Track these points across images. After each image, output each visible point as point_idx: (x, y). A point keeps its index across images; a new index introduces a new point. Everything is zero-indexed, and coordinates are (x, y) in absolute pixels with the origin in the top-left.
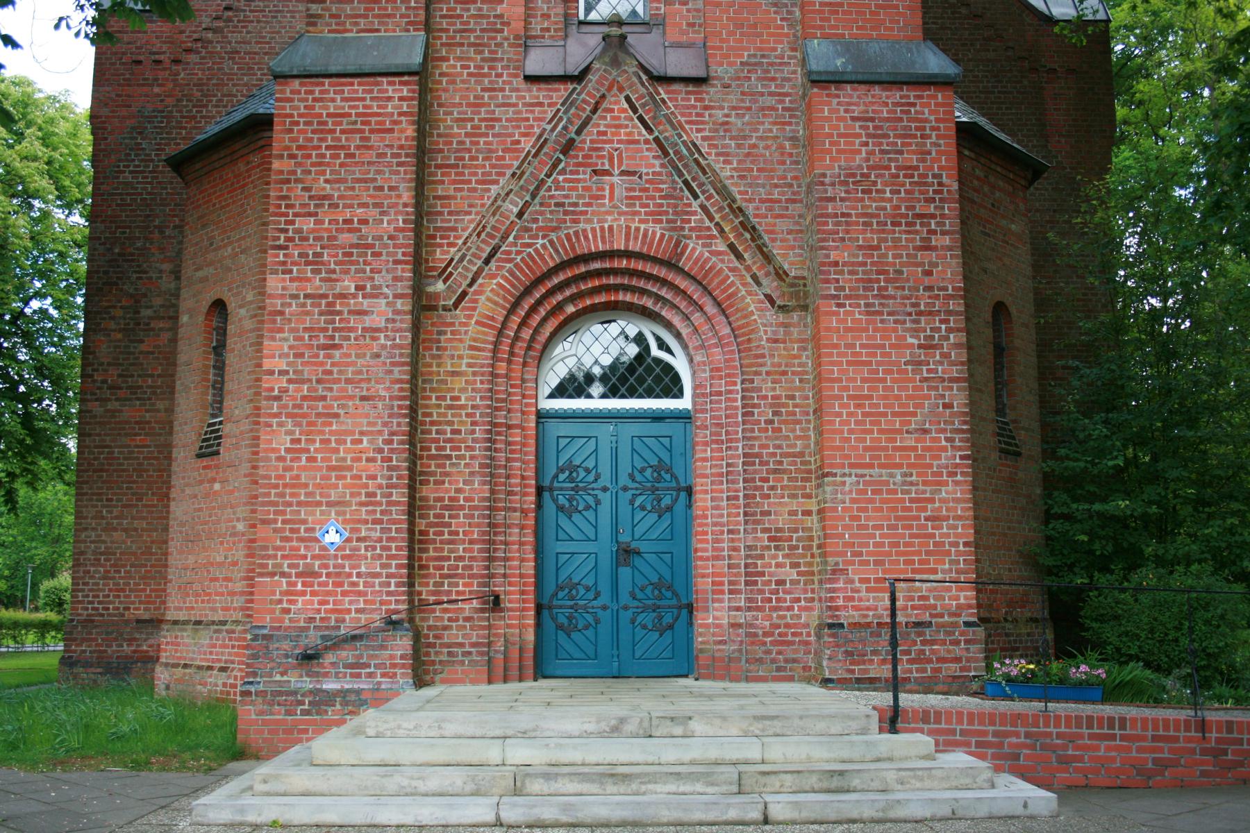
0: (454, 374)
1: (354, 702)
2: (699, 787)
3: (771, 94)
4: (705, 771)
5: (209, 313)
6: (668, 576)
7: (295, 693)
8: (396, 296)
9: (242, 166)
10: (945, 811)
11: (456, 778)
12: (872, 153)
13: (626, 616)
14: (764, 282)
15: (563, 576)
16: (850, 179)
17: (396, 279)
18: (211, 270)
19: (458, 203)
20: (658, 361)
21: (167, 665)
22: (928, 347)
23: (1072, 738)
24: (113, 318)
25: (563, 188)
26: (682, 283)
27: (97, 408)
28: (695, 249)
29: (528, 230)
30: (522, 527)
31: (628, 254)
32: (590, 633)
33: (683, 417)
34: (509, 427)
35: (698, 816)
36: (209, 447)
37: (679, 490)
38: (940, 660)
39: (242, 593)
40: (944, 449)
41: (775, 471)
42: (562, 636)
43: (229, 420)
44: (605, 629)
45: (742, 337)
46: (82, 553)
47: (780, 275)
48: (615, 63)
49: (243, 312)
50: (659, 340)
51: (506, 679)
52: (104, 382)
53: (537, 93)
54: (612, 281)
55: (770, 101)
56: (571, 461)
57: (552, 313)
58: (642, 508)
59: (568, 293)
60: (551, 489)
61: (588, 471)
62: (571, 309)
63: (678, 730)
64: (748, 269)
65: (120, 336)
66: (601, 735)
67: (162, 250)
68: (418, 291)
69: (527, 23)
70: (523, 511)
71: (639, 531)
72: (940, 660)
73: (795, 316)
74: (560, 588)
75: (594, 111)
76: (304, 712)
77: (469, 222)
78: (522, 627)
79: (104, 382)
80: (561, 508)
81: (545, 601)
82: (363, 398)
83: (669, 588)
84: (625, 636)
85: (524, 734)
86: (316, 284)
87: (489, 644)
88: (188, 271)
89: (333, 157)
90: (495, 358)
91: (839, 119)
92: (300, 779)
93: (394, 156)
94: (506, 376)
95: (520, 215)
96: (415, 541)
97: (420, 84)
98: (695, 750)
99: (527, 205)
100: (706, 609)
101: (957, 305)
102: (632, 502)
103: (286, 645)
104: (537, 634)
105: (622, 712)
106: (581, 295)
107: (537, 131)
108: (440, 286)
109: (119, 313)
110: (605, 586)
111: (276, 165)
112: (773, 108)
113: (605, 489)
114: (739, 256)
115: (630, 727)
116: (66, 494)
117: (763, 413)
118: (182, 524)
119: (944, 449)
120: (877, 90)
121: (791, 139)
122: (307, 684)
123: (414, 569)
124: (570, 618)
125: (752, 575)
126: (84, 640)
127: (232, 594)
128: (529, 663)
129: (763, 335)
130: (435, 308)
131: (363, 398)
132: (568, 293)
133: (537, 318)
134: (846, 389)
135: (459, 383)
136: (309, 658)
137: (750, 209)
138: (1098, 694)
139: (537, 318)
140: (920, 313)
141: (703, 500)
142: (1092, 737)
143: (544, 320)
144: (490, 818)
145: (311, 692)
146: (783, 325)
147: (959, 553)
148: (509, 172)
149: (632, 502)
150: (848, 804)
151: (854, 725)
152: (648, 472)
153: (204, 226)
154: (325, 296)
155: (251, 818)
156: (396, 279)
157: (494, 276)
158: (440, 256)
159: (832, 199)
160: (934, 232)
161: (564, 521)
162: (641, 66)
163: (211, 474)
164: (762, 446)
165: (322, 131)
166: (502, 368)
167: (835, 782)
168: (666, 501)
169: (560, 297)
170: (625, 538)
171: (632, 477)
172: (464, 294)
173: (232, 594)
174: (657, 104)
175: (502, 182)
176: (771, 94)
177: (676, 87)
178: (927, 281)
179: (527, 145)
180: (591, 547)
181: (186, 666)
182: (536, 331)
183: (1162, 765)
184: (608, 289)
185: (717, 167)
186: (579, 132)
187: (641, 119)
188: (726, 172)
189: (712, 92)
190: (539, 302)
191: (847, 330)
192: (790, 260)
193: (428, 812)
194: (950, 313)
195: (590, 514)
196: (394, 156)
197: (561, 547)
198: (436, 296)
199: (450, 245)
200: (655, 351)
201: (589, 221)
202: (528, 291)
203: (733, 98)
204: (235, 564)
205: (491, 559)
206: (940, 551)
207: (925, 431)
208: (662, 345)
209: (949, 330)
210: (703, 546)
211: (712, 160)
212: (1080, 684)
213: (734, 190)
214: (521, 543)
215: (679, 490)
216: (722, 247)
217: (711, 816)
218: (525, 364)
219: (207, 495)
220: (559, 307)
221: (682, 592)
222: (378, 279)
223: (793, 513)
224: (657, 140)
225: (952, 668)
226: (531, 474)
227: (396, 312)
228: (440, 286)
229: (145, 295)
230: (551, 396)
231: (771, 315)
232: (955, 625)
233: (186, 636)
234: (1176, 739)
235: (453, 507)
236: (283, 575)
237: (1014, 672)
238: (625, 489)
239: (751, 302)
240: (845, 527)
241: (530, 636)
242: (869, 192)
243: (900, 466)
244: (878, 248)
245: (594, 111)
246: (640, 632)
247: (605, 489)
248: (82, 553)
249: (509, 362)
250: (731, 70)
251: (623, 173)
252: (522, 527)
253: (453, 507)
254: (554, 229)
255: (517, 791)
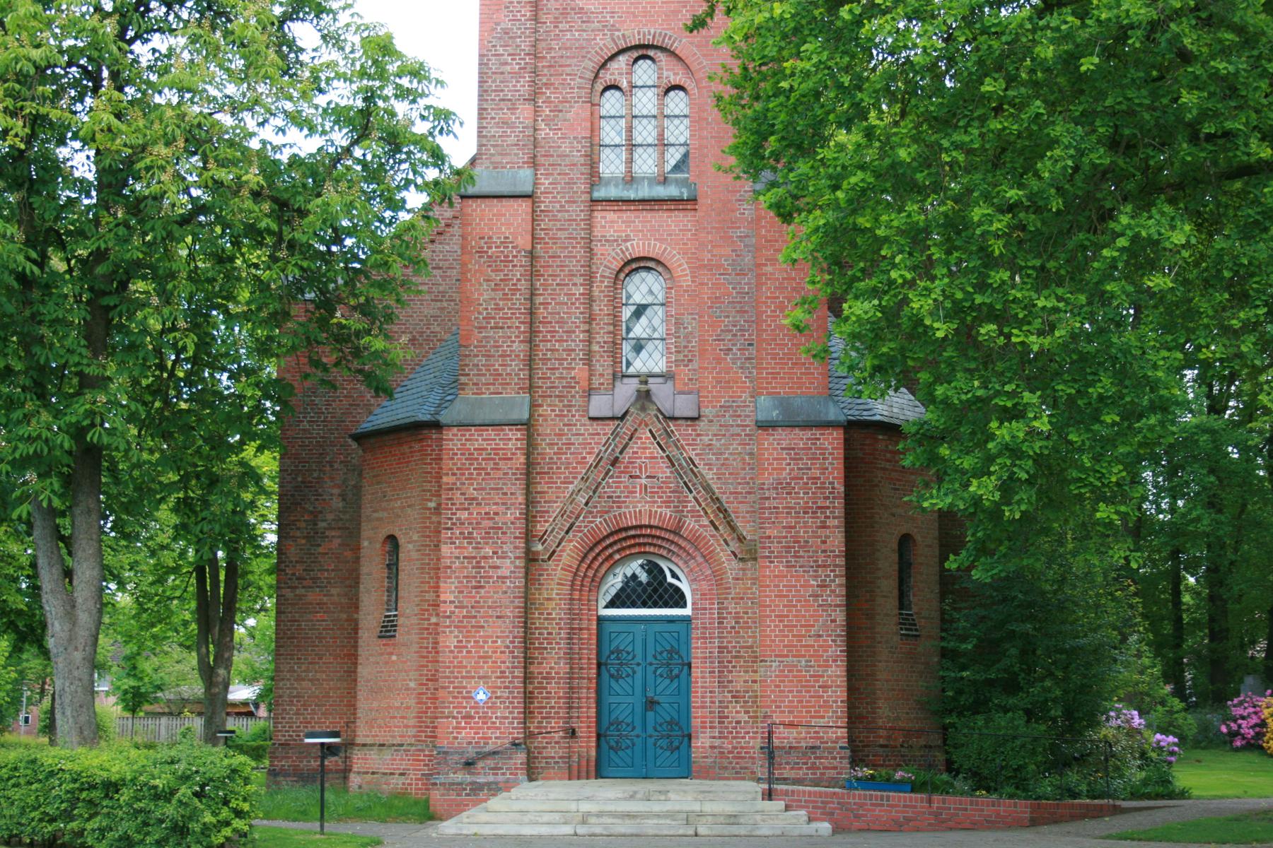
0: (549, 599)
1: (494, 789)
2: (668, 821)
3: (738, 426)
4: (670, 815)
5: (384, 542)
6: (676, 717)
7: (460, 784)
8: (517, 558)
9: (406, 449)
10: (779, 832)
11: (557, 817)
12: (792, 469)
13: (650, 741)
14: (731, 543)
15: (613, 717)
16: (779, 486)
17: (516, 548)
18: (385, 514)
19: (551, 495)
20: (671, 585)
21: (359, 773)
22: (823, 586)
23: (861, 805)
24: (298, 529)
25: (613, 486)
26: (683, 544)
27: (289, 594)
28: (690, 523)
29: (591, 512)
30: (589, 688)
31: (651, 527)
32: (629, 751)
33: (686, 620)
34: (581, 629)
35: (665, 832)
36: (388, 630)
37: (683, 665)
38: (825, 768)
39: (414, 727)
40: (830, 646)
41: (736, 657)
42: (612, 753)
43: (402, 616)
44: (638, 748)
45: (718, 576)
46: (280, 697)
47: (741, 539)
48: (643, 409)
49: (410, 546)
50: (671, 571)
51: (579, 778)
52: (294, 574)
53: (597, 427)
54: (641, 540)
55: (738, 430)
56: (618, 647)
57: (607, 559)
58: (661, 676)
59: (615, 548)
60: (606, 664)
61: (628, 653)
62: (617, 557)
63: (663, 798)
64: (721, 535)
65: (303, 541)
66: (625, 799)
67: (332, 479)
68: (528, 551)
69: (590, 380)
70: (589, 679)
71: (659, 689)
72: (825, 768)
73: (749, 564)
74: (611, 724)
75: (630, 439)
76: (467, 795)
77: (556, 508)
78: (588, 747)
79: (294, 574)
80: (612, 676)
81: (602, 732)
82: (498, 617)
83: (677, 724)
84: (650, 753)
85: (588, 798)
86: (470, 551)
87: (569, 757)
88: (366, 511)
89: (479, 474)
90: (572, 590)
91: (775, 449)
92: (484, 817)
93: (514, 474)
94: (580, 600)
95: (587, 504)
96: (528, 697)
97: (528, 430)
98: (668, 807)
99: (590, 497)
100: (697, 738)
101: (841, 561)
102: (655, 672)
103: (456, 757)
104: (597, 752)
105: (634, 788)
106: (623, 549)
107: (596, 451)
108: (540, 547)
109: (303, 525)
110: (638, 723)
111: (445, 479)
112: (739, 435)
113: (638, 664)
114: (716, 528)
115: (638, 796)
116: (15, 602)
117: (729, 622)
118: (368, 681)
119: (830, 646)
120: (797, 431)
121: (750, 454)
122: (469, 778)
123: (527, 713)
124: (617, 742)
125: (722, 718)
126: (284, 758)
127: (406, 727)
128: (592, 769)
129: (730, 576)
130: (536, 560)
131: (498, 617)
132: (615, 548)
133: (597, 563)
134: (773, 611)
135: (552, 605)
136: (469, 764)
137: (724, 499)
138: (909, 788)
139: (597, 563)
140: (819, 566)
141: (696, 673)
142: (872, 805)
143: (602, 564)
144: (572, 832)
145: (471, 783)
146: (743, 570)
147: (838, 707)
148: (580, 477)
149: (655, 672)
150: (735, 830)
151: (750, 796)
152: (665, 654)
153: (378, 483)
154: (475, 558)
155: (465, 832)
156: (516, 548)
157: (571, 541)
158: (540, 528)
159: (768, 498)
160: (828, 517)
161: (613, 683)
162: (659, 410)
163: (389, 649)
164: (729, 642)
165: (471, 459)
166: (576, 595)
167: (732, 820)
168: (676, 672)
169: (610, 551)
170: (650, 694)
171: (655, 657)
172: (554, 552)
173: (406, 727)
174: (669, 435)
175: (576, 482)
176: (738, 426)
177: (679, 422)
178: (823, 547)
179: (591, 459)
180: (630, 700)
181: (373, 773)
182: (597, 571)
183: (908, 820)
184: (640, 545)
185: (704, 472)
186: (621, 453)
187: (658, 443)
188: (709, 476)
189: (702, 424)
190: (598, 554)
191: (775, 576)
192: (745, 529)
193: (544, 830)
194: (836, 566)
195: (629, 680)
196: (514, 474)
197: (612, 699)
198: (538, 553)
199: (546, 521)
200: (670, 579)
201: (627, 507)
202: (591, 549)
203: (715, 428)
204: (408, 708)
205: (570, 708)
206: (826, 705)
207: (820, 636)
208: (674, 575)
209: (836, 576)
210: (696, 701)
211: (702, 468)
212: (897, 782)
213: (714, 487)
214: (588, 698)
215: (683, 665)
216: (706, 523)
217: (671, 833)
218: (590, 591)
219: (387, 663)
220: (611, 556)
221: (684, 727)
222: (505, 548)
223: (746, 682)
224: (668, 456)
225: (831, 773)
226: (594, 656)
227: (516, 567)
228: (540, 547)
229: (321, 512)
230: (606, 607)
231: (735, 564)
232: (834, 748)
233: (373, 754)
234: (915, 807)
235: (548, 678)
236: (454, 717)
237: (860, 774)
238: (651, 664)
239: (723, 555)
240: (772, 691)
241: (593, 753)
242: (789, 493)
243: (804, 656)
244: (794, 527)
245: (630, 439)
246: (659, 751)
247: (638, 664)
248: (280, 697)
249: (581, 590)
250: (714, 410)
251: (648, 477)
252: (589, 688)
253: (548, 678)
254: (606, 512)
255: (584, 822)
